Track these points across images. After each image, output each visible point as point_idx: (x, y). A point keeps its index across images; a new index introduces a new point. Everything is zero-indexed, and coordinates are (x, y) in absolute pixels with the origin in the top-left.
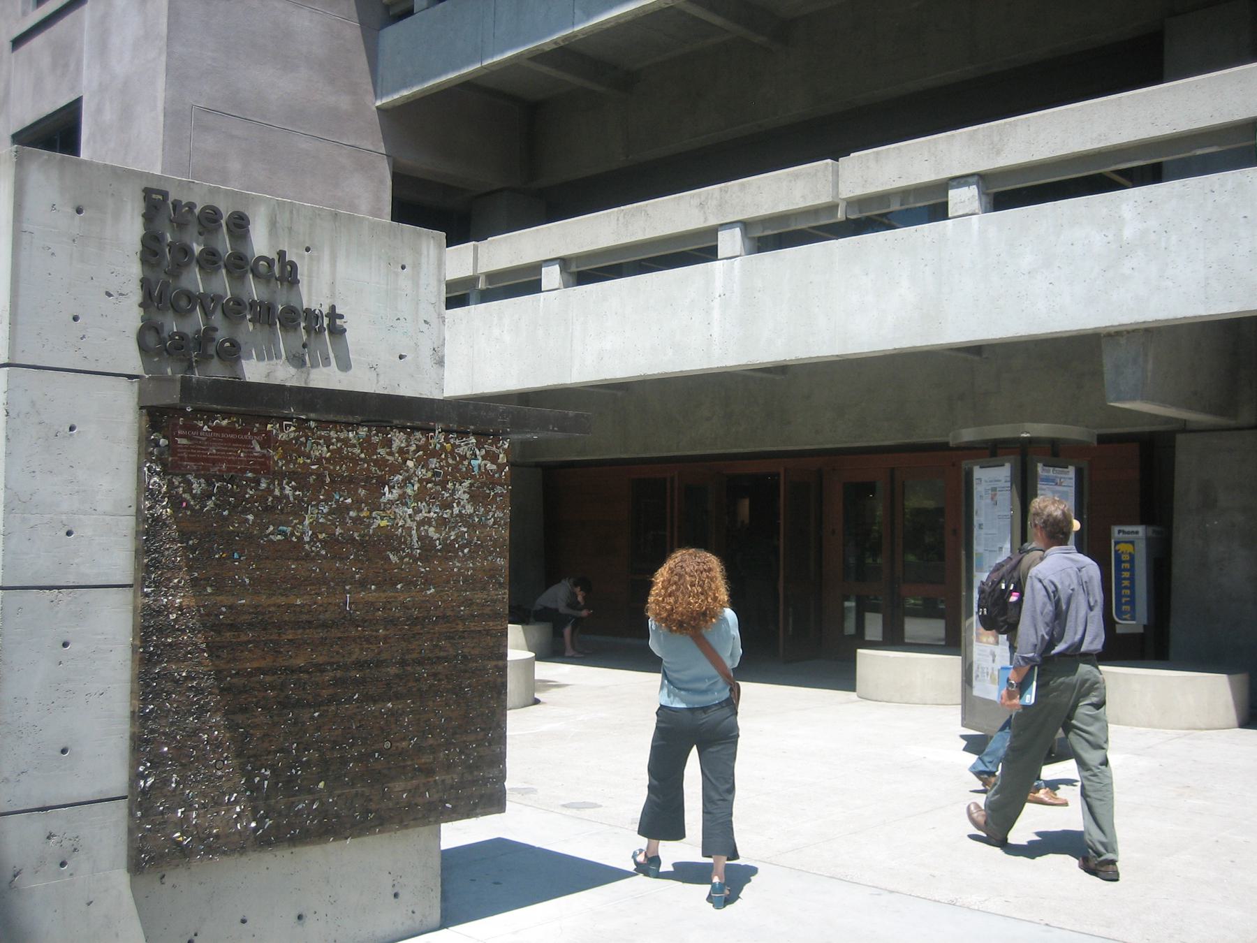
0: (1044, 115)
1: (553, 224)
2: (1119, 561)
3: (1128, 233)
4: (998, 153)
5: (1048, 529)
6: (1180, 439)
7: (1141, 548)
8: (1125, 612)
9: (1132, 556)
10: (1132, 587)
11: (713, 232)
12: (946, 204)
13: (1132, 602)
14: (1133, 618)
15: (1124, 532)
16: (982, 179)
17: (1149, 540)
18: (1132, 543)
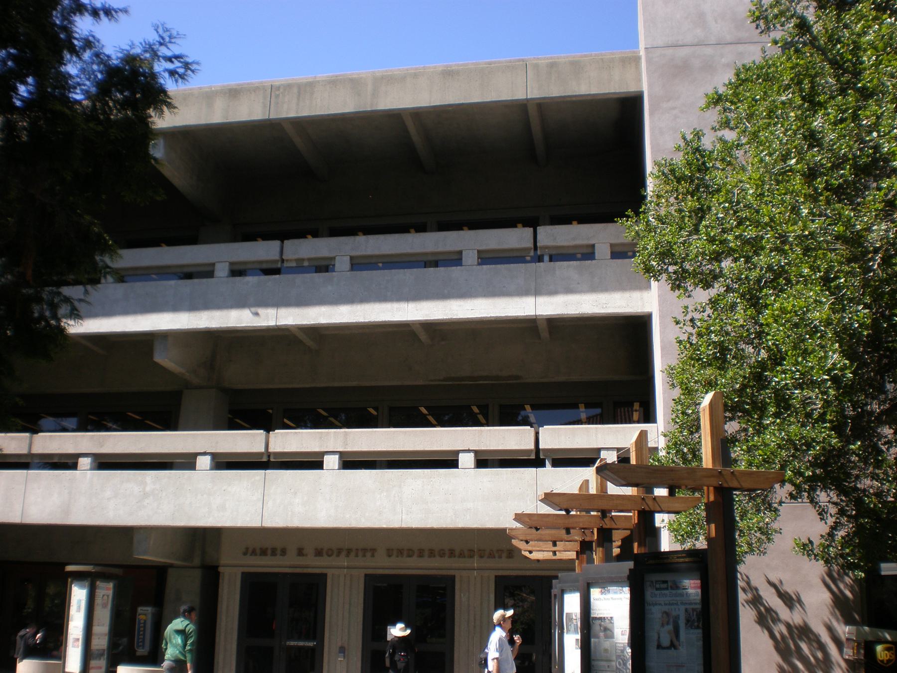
0: (76, 436)
1: (462, 428)
2: (140, 623)
3: (148, 489)
4: (102, 446)
5: (607, 621)
6: (170, 571)
7: (150, 616)
8: (140, 646)
9: (145, 621)
10: (144, 635)
11: (195, 455)
12: (457, 461)
13: (143, 641)
14: (143, 648)
15: (142, 610)
16: (95, 456)
17: (153, 614)
18: (145, 615)
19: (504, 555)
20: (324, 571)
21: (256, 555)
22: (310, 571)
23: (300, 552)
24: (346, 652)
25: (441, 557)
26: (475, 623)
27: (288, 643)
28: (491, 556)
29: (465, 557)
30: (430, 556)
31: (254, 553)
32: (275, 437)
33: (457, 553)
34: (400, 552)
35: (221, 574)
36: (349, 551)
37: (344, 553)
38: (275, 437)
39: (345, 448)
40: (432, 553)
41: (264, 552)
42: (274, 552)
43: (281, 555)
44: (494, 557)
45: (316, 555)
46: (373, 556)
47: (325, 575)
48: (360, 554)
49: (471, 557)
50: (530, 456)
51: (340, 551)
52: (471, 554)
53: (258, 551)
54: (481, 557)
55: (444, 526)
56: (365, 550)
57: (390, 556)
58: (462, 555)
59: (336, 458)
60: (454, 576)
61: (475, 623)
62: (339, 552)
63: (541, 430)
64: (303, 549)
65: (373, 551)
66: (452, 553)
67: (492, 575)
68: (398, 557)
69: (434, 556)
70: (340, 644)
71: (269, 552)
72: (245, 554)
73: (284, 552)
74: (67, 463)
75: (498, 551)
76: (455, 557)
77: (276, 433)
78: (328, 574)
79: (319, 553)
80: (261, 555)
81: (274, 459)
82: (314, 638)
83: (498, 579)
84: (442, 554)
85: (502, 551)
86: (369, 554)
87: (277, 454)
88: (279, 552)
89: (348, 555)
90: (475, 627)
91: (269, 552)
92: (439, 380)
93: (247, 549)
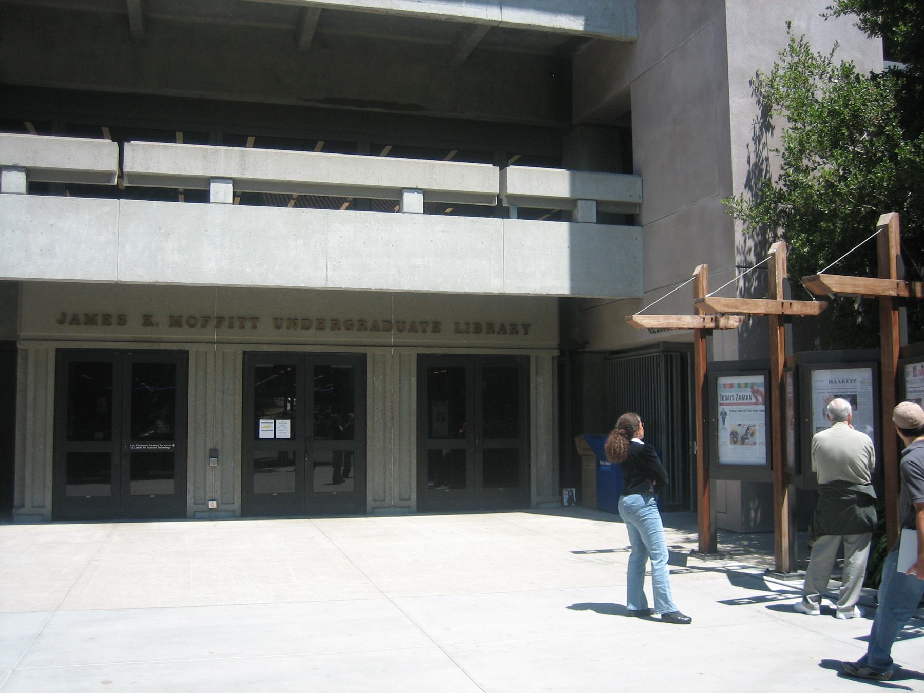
11: (400, 192)
19: (429, 328)
20: (185, 347)
21: (78, 323)
22: (163, 346)
23: (148, 321)
24: (220, 454)
25: (348, 329)
26: (393, 413)
27: (133, 447)
28: (413, 329)
29: (379, 330)
30: (332, 329)
31: (75, 320)
32: (133, 150)
33: (497, 329)
34: (293, 322)
35: (20, 353)
36: (220, 320)
37: (213, 322)
38: (133, 150)
39: (243, 174)
40: (335, 325)
41: (90, 320)
42: (107, 320)
43: (119, 324)
44: (417, 331)
45: (171, 326)
46: (254, 327)
47: (528, 358)
48: (237, 324)
49: (388, 330)
50: (491, 203)
51: (206, 320)
52: (387, 326)
53: (82, 319)
54: (400, 330)
55: (385, 288)
56: (242, 319)
57: (278, 327)
58: (375, 328)
59: (229, 188)
60: (365, 355)
61: (393, 413)
62: (206, 321)
63: (126, 145)
64: (151, 316)
65: (255, 320)
66: (362, 325)
67: (413, 353)
68: (289, 328)
69: (339, 329)
70: (210, 445)
71: (99, 319)
72: (61, 322)
73: (122, 320)
74: (177, 189)
75: (421, 323)
76: (366, 329)
77: (132, 145)
78: (190, 352)
79: (175, 322)
80: (86, 324)
81: (129, 183)
82: (169, 438)
83: (421, 357)
84: (349, 326)
85: (426, 323)
86: (248, 324)
87: (134, 176)
88: (114, 320)
89: (218, 326)
90: (392, 418)
91: (99, 319)
92: (860, 466)
93: (64, 314)
